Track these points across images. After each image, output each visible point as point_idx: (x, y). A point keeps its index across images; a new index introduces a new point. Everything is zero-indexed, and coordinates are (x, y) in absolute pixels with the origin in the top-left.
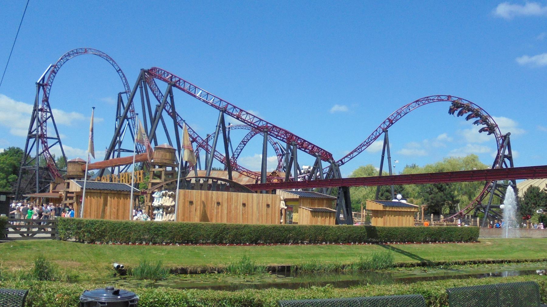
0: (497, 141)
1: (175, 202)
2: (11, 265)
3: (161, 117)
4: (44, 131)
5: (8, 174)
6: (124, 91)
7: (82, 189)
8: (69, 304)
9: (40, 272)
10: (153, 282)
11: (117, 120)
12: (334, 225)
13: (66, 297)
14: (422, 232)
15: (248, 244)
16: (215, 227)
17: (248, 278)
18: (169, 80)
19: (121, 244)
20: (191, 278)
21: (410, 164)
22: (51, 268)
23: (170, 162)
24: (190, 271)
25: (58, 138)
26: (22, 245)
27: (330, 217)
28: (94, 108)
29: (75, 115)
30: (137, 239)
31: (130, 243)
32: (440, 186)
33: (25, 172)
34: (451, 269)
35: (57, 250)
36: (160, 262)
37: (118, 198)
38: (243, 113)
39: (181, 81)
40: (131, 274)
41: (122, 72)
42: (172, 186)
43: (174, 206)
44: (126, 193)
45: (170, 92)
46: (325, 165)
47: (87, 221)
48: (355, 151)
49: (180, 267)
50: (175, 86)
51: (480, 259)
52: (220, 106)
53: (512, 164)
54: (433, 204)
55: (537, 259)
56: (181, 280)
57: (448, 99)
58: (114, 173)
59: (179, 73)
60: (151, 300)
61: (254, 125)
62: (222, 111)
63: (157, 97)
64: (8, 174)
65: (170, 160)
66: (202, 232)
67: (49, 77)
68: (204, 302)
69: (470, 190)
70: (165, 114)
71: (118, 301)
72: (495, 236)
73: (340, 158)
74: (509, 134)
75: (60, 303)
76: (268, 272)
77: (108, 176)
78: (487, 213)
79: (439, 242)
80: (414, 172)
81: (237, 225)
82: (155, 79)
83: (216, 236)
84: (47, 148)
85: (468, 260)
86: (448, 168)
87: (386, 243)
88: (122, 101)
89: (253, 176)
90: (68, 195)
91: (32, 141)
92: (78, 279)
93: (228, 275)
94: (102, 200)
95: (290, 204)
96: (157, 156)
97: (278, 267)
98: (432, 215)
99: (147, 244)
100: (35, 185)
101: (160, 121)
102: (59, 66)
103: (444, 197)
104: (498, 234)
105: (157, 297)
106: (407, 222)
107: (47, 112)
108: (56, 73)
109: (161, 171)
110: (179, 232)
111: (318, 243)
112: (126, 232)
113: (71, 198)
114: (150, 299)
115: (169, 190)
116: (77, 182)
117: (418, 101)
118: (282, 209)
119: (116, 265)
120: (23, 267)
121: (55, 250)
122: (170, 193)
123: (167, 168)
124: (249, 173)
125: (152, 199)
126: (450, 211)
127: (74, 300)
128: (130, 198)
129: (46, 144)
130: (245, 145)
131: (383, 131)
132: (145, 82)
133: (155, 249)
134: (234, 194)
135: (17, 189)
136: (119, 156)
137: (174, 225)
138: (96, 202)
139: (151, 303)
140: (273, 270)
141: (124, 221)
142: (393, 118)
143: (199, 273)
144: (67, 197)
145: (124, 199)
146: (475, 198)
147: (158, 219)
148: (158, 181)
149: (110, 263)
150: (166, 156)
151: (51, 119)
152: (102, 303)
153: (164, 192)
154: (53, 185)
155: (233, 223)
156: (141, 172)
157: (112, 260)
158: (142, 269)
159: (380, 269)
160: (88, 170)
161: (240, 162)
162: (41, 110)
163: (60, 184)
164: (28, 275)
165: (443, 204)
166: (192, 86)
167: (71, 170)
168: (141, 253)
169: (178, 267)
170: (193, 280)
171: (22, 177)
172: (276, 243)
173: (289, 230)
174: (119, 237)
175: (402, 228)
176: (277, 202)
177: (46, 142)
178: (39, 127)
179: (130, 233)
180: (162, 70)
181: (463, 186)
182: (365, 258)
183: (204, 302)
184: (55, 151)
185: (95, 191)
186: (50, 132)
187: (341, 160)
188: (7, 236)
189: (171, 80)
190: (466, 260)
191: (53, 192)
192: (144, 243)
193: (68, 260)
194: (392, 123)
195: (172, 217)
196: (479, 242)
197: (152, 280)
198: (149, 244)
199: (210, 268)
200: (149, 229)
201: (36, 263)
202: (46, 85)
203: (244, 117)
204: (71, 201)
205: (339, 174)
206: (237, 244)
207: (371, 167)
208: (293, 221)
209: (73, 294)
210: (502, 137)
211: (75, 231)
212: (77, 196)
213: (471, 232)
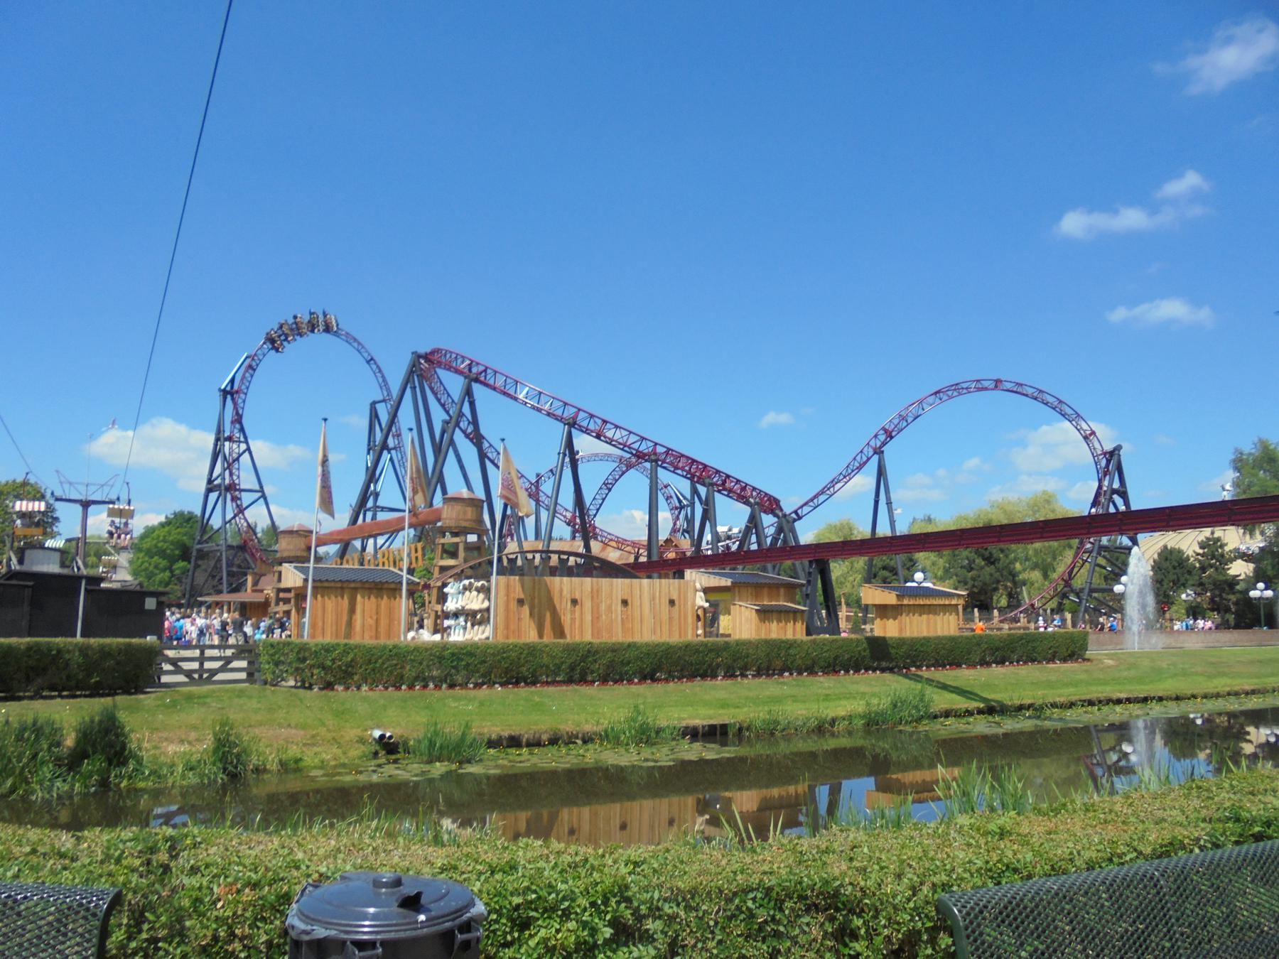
0: (1096, 463)
1: (489, 600)
2: (166, 739)
3: (452, 443)
4: (235, 478)
5: (172, 560)
6: (381, 398)
7: (306, 580)
8: (256, 919)
9: (224, 753)
10: (454, 767)
11: (369, 453)
12: (805, 638)
13: (248, 896)
14: (978, 645)
15: (636, 680)
16: (570, 649)
17: (647, 752)
18: (466, 370)
19: (386, 688)
20: (529, 757)
21: (920, 516)
22: (245, 744)
23: (474, 525)
24: (527, 740)
25: (262, 490)
26: (190, 697)
27: (795, 621)
28: (325, 420)
29: (295, 451)
30: (416, 678)
31: (404, 687)
32: (987, 554)
33: (202, 555)
34: (1050, 719)
35: (259, 705)
36: (467, 725)
37: (376, 597)
38: (609, 426)
39: (489, 371)
40: (407, 751)
41: (375, 363)
42: (480, 571)
43: (488, 610)
44: (393, 586)
45: (468, 393)
46: (768, 520)
47: (317, 645)
49: (506, 734)
50: (477, 380)
51: (1102, 696)
52: (565, 416)
53: (1127, 503)
54: (975, 590)
55: (1215, 691)
56: (510, 761)
57: (996, 387)
58: (367, 550)
59: (485, 356)
60: (517, 900)
61: (630, 448)
62: (568, 424)
63: (443, 406)
64: (172, 560)
65: (474, 521)
66: (546, 660)
67: (243, 377)
68: (684, 899)
69: (1044, 560)
70: (459, 436)
71: (419, 932)
72: (1110, 647)
73: (795, 508)
74: (1118, 448)
75: (228, 917)
76: (683, 738)
77: (356, 556)
78: (1084, 602)
79: (1011, 663)
80: (930, 529)
81: (614, 644)
82: (438, 370)
83: (572, 668)
84: (241, 510)
85: (1077, 698)
86: (1000, 519)
87: (908, 669)
88: (377, 416)
89: (629, 549)
90: (282, 595)
91: (213, 496)
92: (302, 764)
93: (603, 748)
94: (345, 602)
95: (714, 597)
96: (450, 516)
97: (703, 727)
98: (976, 610)
99: (438, 687)
100: (221, 579)
101: (451, 452)
102: (261, 357)
103: (997, 575)
104: (1117, 644)
105: (534, 887)
106: (946, 626)
107: (240, 442)
108: (254, 370)
109: (457, 544)
110: (500, 662)
111: (773, 674)
112: (396, 665)
113: (287, 601)
114: (512, 894)
115: (478, 579)
116: (296, 567)
117: (936, 393)
118: (699, 608)
119: (377, 733)
120: (190, 743)
121: (254, 706)
122: (479, 584)
123: (469, 536)
124: (621, 543)
125: (443, 598)
126: (1009, 602)
127: (273, 907)
128: (401, 597)
129: (239, 502)
130: (610, 490)
131: (875, 453)
132: (421, 377)
133: (455, 699)
134: (605, 582)
135: (188, 589)
136: (374, 517)
137: (488, 646)
138: (333, 606)
139: (517, 907)
140: (694, 734)
141: (390, 643)
142: (893, 426)
143: (544, 745)
144: (278, 600)
145: (389, 598)
146: (1055, 576)
147: (457, 637)
148: (451, 562)
149: (366, 730)
150: (465, 513)
151: (247, 454)
152: (361, 945)
153: (466, 582)
154: (253, 579)
155: (604, 640)
156: (420, 545)
157: (369, 723)
158: (430, 741)
159: (907, 722)
160: (317, 546)
161: (599, 522)
162: (230, 439)
163: (265, 575)
164: (199, 761)
165: (996, 589)
166: (509, 381)
167: (284, 546)
168: (427, 708)
169: (502, 733)
170: (534, 760)
171: (197, 566)
172: (692, 677)
173: (717, 650)
174: (382, 675)
175: (938, 638)
176: (690, 594)
177: (240, 499)
178: (225, 470)
179: (403, 667)
180: (451, 352)
181: (1031, 552)
182: (875, 701)
183: (684, 899)
184: (257, 516)
185: (332, 584)
186: (246, 480)
187: (796, 512)
188: (159, 679)
189: (470, 370)
190: (1073, 698)
191: (253, 591)
192: (431, 685)
193: (280, 725)
194: (890, 436)
195: (483, 632)
196: (1088, 660)
197: (452, 763)
198: (440, 688)
199: (567, 733)
200: (441, 658)
201: (215, 734)
202: (237, 392)
203: (610, 434)
204: (286, 608)
205: (796, 538)
206: (616, 682)
207: (848, 524)
208: (721, 631)
209: (270, 885)
210: (1105, 454)
211: (294, 665)
212: (297, 596)
213: (1073, 641)
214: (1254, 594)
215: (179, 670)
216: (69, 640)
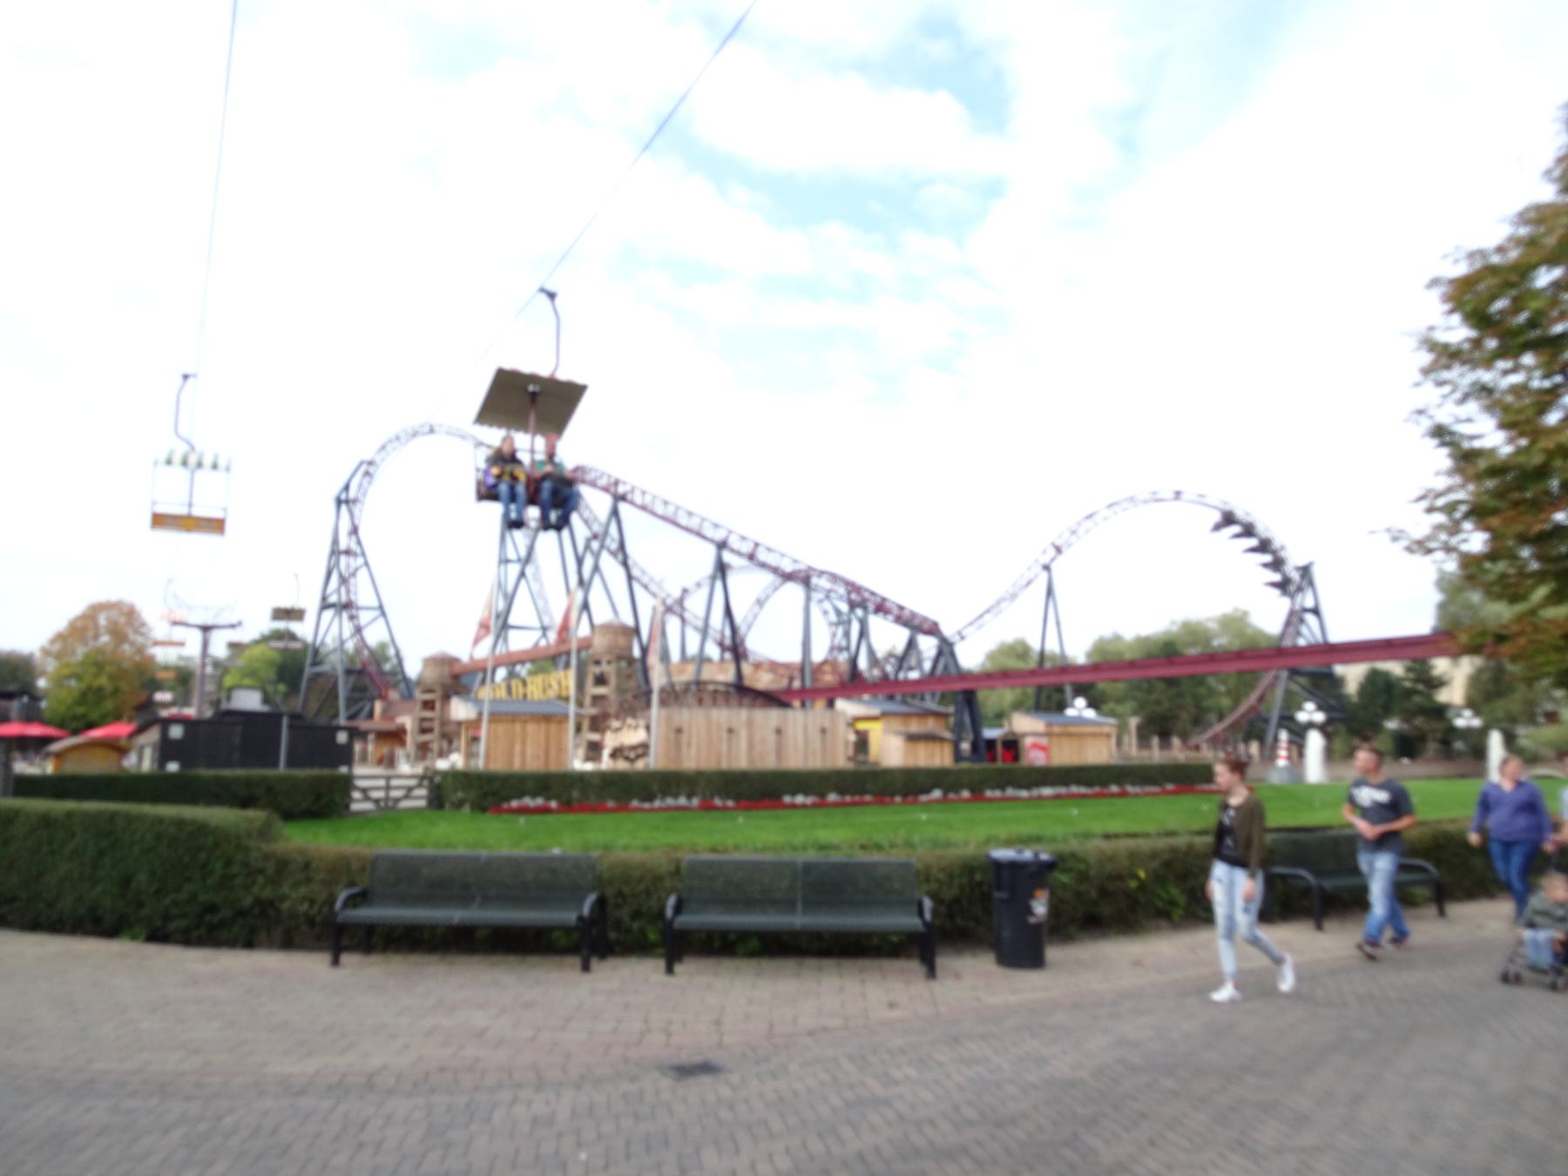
7: (480, 714)
25: (381, 608)
45: (615, 513)
124: (774, 666)
162: (348, 552)
186: (363, 594)
187: (959, 633)
215: (367, 798)
216: (257, 772)
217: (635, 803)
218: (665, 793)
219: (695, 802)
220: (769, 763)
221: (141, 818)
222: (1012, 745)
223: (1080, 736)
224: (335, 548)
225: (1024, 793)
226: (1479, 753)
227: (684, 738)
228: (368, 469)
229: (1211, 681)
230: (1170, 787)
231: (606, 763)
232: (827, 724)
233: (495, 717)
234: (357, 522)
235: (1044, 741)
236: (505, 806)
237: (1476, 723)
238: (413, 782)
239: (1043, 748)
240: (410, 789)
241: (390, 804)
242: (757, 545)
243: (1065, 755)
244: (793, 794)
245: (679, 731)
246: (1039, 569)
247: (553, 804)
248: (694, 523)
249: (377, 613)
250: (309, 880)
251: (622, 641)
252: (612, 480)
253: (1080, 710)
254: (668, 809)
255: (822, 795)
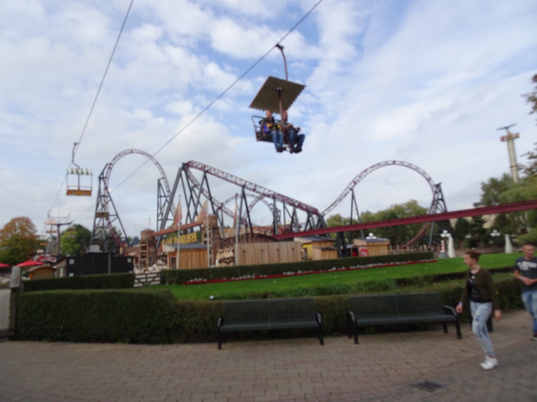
7: (176, 250)
25: (117, 215)
45: (205, 177)
48: (332, 205)
186: (111, 211)
194: (355, 183)
214: (493, 235)
215: (140, 282)
216: (102, 275)
217: (233, 278)
218: (242, 275)
219: (253, 276)
220: (276, 261)
221: (125, 294)
222: (355, 250)
223: (378, 246)
224: (100, 194)
225: (363, 267)
226: (501, 244)
227: (246, 254)
228: (110, 166)
229: (406, 226)
230: (410, 262)
231: (217, 265)
232: (294, 246)
233: (182, 250)
234: (107, 185)
235: (366, 248)
236: (188, 282)
237: (498, 234)
238: (155, 275)
239: (366, 251)
240: (154, 278)
241: (148, 283)
242: (256, 186)
243: (373, 253)
244: (287, 271)
245: (244, 252)
246: (348, 190)
247: (205, 280)
248: (233, 179)
249: (115, 217)
250: (195, 315)
251: (214, 221)
252: (203, 166)
253: (371, 237)
254: (245, 279)
255: (296, 271)
